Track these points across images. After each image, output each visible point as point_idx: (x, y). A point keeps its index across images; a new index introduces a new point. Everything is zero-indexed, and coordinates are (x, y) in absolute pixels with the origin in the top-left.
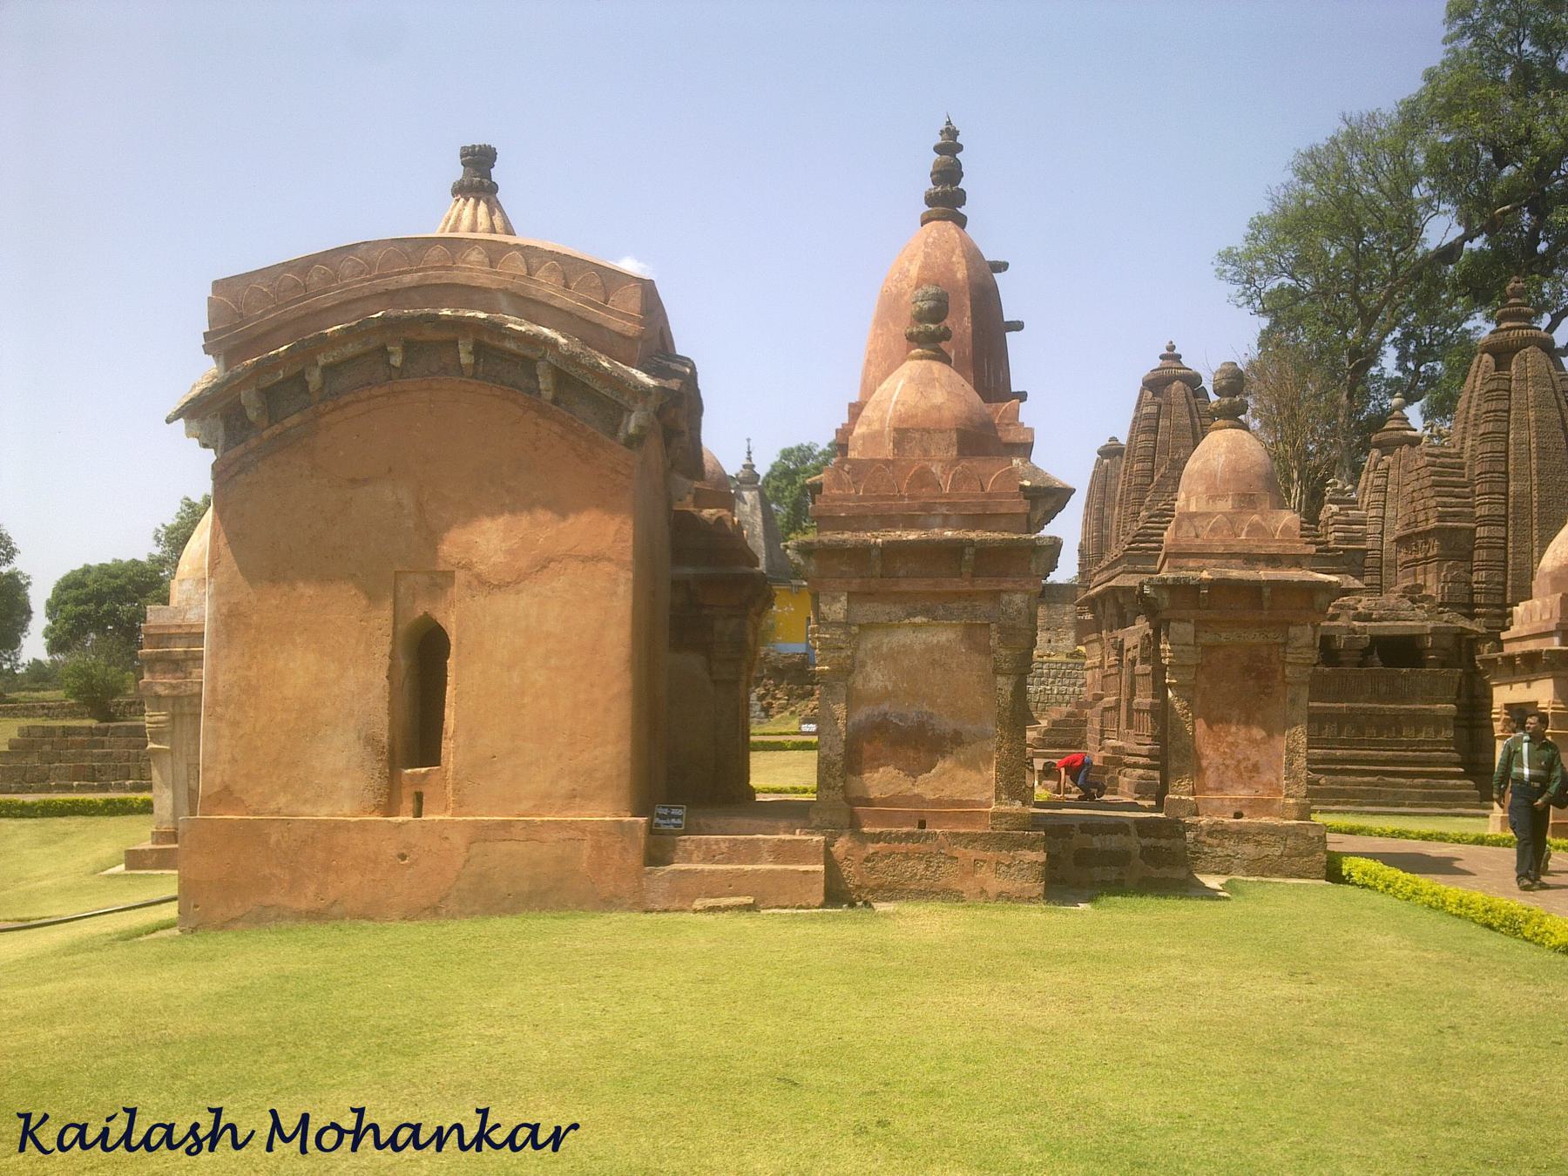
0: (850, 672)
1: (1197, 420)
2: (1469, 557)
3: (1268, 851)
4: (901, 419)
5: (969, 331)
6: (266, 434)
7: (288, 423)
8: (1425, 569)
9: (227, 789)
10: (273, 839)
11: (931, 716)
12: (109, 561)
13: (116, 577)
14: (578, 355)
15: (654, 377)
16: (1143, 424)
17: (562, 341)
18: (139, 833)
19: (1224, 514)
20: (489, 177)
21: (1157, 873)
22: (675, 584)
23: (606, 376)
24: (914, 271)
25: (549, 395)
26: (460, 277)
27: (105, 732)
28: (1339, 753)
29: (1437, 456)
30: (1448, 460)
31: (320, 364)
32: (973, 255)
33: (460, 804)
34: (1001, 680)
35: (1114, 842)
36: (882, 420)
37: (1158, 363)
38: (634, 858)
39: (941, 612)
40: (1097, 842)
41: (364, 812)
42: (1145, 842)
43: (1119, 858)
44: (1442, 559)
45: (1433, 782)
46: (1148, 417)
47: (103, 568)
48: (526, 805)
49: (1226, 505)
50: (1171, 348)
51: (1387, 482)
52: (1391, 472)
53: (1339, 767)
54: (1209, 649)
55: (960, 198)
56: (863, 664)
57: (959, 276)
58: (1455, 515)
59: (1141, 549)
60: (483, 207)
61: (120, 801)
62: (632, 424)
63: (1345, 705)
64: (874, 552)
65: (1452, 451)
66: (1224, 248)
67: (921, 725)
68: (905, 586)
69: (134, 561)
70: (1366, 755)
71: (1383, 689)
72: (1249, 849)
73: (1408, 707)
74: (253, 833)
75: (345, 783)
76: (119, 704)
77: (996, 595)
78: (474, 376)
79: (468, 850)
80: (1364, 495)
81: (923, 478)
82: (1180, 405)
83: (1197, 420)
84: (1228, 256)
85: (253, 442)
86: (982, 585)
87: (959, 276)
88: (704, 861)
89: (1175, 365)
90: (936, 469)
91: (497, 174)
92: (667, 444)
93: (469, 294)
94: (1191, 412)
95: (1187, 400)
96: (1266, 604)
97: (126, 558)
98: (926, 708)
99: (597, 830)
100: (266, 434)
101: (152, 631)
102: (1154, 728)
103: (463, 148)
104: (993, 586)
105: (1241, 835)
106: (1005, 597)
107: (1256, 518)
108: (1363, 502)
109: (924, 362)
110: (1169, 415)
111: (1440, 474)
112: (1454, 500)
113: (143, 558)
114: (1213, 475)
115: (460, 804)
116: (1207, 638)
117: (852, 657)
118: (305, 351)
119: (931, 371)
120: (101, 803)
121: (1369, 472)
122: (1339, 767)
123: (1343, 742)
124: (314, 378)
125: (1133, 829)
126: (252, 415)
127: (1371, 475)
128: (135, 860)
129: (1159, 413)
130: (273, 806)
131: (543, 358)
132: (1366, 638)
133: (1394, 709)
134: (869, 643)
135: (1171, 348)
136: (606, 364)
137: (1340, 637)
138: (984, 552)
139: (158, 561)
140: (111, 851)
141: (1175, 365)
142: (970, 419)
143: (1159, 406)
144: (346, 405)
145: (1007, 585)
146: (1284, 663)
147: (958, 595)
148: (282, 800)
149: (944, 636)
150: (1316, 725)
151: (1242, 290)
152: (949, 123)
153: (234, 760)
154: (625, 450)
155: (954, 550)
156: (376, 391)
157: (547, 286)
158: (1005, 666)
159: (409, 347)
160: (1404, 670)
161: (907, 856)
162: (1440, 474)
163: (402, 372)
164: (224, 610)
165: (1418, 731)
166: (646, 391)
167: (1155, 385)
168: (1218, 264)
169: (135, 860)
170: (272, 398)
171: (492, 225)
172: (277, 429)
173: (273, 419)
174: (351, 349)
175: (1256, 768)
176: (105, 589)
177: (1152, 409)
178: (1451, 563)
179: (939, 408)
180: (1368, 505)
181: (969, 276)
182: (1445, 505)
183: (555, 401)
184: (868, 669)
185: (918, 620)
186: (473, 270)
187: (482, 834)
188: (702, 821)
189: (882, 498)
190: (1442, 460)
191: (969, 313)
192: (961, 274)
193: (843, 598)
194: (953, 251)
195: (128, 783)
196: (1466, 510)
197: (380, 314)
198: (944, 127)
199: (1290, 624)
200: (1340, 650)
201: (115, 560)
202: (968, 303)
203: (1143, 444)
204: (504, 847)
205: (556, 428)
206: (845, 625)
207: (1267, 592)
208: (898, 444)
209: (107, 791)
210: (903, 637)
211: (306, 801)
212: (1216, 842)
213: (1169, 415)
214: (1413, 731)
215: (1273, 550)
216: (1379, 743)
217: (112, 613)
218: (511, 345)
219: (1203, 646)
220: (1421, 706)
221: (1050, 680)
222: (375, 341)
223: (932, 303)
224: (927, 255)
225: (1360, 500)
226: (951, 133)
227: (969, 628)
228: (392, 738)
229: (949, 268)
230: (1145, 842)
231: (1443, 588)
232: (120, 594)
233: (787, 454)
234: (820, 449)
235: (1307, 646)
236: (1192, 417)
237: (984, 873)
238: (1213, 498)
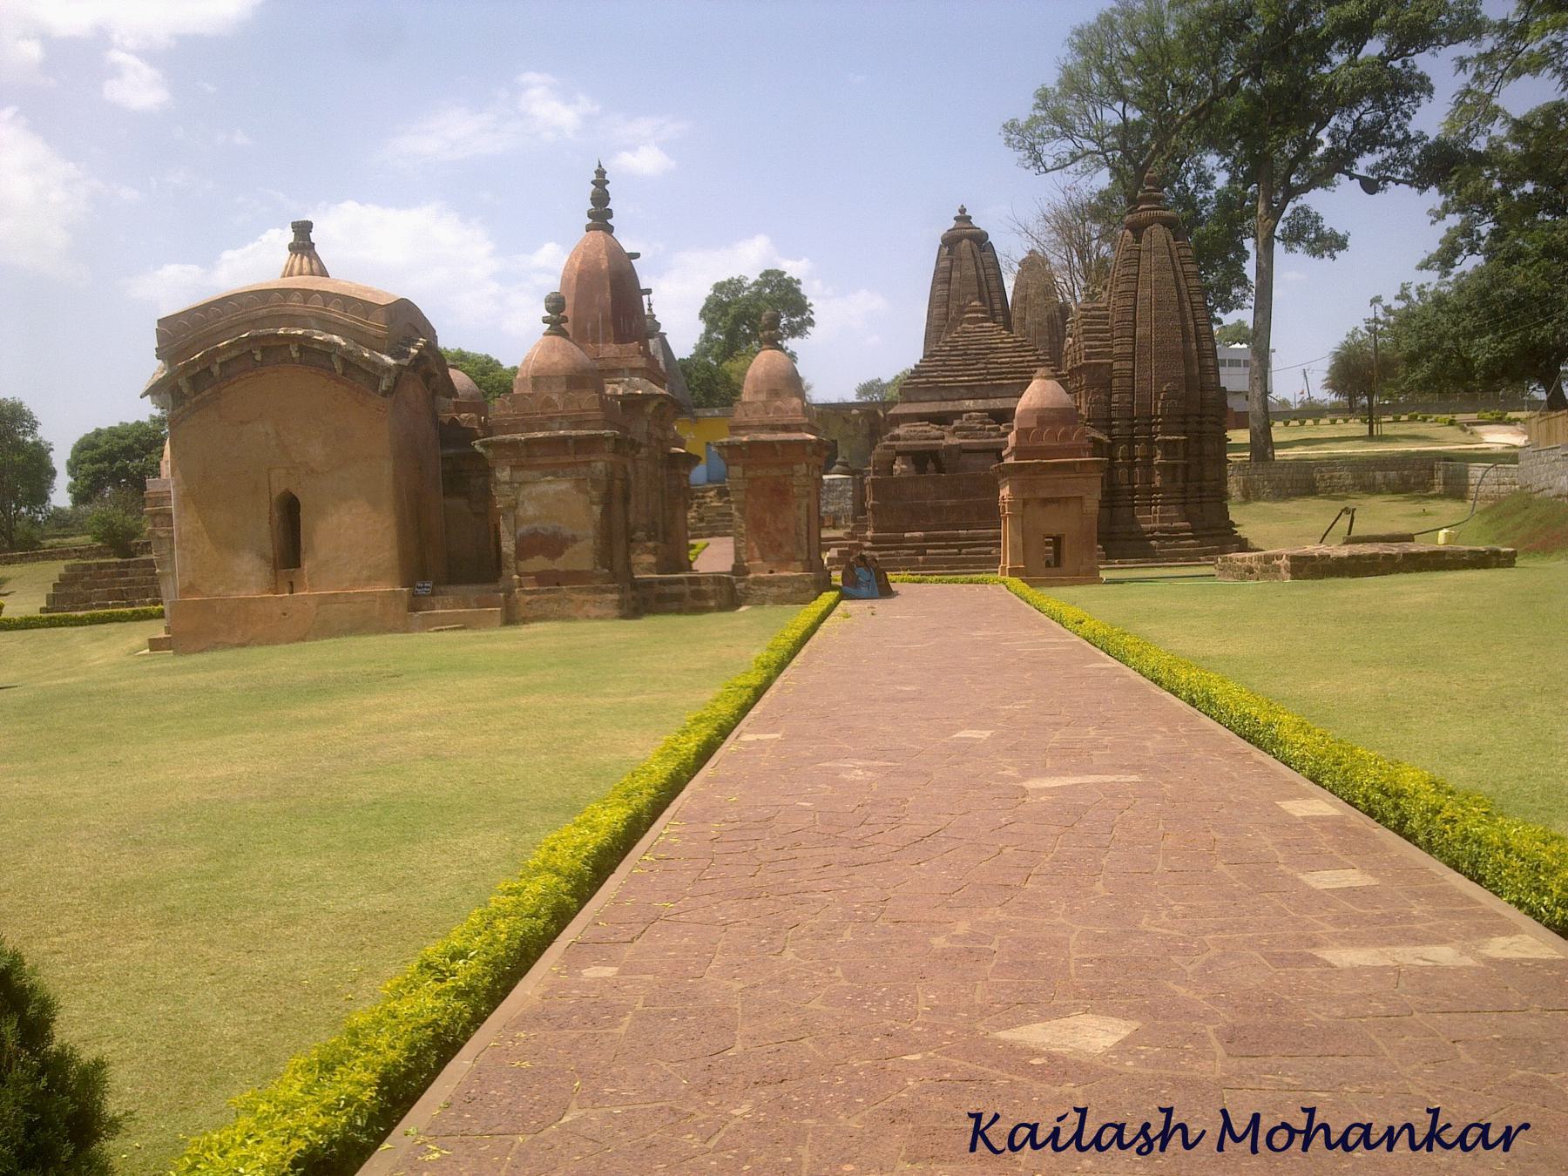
0: (515, 508)
3: (784, 590)
4: (536, 371)
6: (194, 400)
10: (218, 608)
11: (560, 528)
12: (117, 425)
15: (394, 358)
17: (343, 343)
20: (310, 240)
21: (699, 604)
22: (445, 459)
24: (577, 265)
26: (288, 310)
27: (127, 565)
29: (1089, 310)
30: (1097, 313)
32: (617, 253)
34: (595, 507)
35: (676, 589)
37: (952, 224)
39: (561, 473)
40: (667, 589)
41: (264, 593)
42: (693, 588)
43: (679, 597)
44: (1090, 386)
47: (112, 431)
48: (347, 584)
49: (762, 397)
50: (963, 210)
54: (752, 480)
55: (610, 214)
56: (523, 502)
57: (603, 267)
58: (1098, 354)
60: (306, 259)
61: (143, 611)
65: (1102, 305)
68: (539, 461)
69: (138, 422)
72: (775, 590)
75: (252, 579)
76: (138, 544)
77: (588, 463)
81: (548, 402)
84: (1011, 127)
86: (580, 458)
87: (603, 267)
88: (441, 608)
90: (555, 397)
92: (427, 383)
93: (293, 320)
97: (131, 421)
100: (194, 400)
101: (151, 496)
103: (293, 223)
104: (585, 458)
106: (593, 464)
107: (778, 403)
111: (1090, 324)
112: (1097, 343)
113: (145, 419)
115: (312, 586)
116: (750, 474)
117: (516, 500)
118: (209, 357)
119: (554, 341)
120: (130, 613)
124: (216, 370)
125: (686, 581)
126: (185, 391)
128: (155, 645)
130: (216, 592)
131: (334, 353)
134: (525, 491)
135: (963, 210)
136: (367, 355)
140: (139, 642)
141: (966, 226)
142: (575, 368)
143: (952, 261)
144: (234, 383)
145: (592, 458)
148: (221, 589)
149: (564, 485)
151: (1028, 155)
152: (600, 166)
153: (194, 570)
156: (250, 374)
157: (335, 313)
158: (596, 500)
159: (264, 350)
161: (548, 601)
162: (1090, 324)
163: (262, 363)
164: (181, 493)
166: (388, 369)
167: (950, 242)
169: (155, 645)
170: (194, 381)
171: (312, 269)
172: (199, 397)
173: (197, 392)
174: (234, 353)
175: (780, 545)
179: (556, 364)
181: (609, 267)
182: (1091, 347)
183: (344, 374)
184: (526, 505)
185: (549, 478)
187: (324, 600)
188: (442, 589)
189: (527, 414)
190: (1093, 313)
191: (609, 290)
192: (604, 266)
193: (508, 469)
194: (600, 251)
196: (1106, 350)
198: (597, 168)
199: (793, 463)
201: (121, 423)
202: (608, 283)
205: (345, 387)
206: (511, 483)
207: (778, 447)
209: (133, 606)
211: (233, 589)
217: (124, 469)
222: (246, 349)
223: (554, 304)
224: (585, 255)
226: (601, 173)
228: (274, 554)
229: (597, 263)
230: (693, 588)
232: (128, 452)
233: (719, 287)
234: (750, 282)
235: (804, 476)
236: (977, 269)
238: (756, 392)
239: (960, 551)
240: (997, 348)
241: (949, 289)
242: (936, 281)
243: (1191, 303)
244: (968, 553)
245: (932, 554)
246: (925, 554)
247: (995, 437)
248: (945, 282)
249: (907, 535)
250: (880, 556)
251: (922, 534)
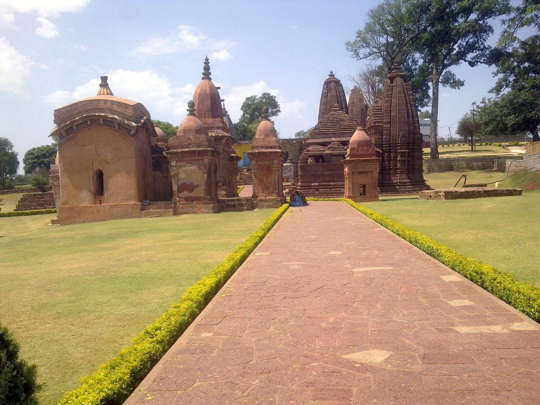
0: (177, 175)
3: (270, 203)
4: (185, 128)
5: (210, 104)
6: (67, 138)
7: (70, 136)
9: (66, 201)
10: (75, 209)
11: (193, 182)
12: (40, 146)
13: (42, 151)
14: (121, 121)
15: (136, 123)
17: (118, 118)
18: (54, 217)
19: (262, 138)
21: (241, 208)
22: (153, 158)
23: (126, 124)
25: (117, 128)
26: (99, 107)
27: (44, 195)
29: (375, 107)
30: (378, 108)
31: (75, 124)
33: (107, 202)
34: (205, 175)
35: (233, 203)
36: (181, 128)
37: (328, 77)
38: (138, 210)
40: (230, 203)
41: (91, 204)
43: (234, 206)
44: (375, 133)
47: (39, 149)
49: (263, 137)
50: (332, 72)
54: (259, 165)
55: (210, 74)
56: (180, 173)
57: (208, 92)
58: (378, 122)
59: (321, 132)
60: (105, 89)
62: (132, 133)
64: (179, 153)
66: (347, 41)
67: (191, 184)
68: (186, 159)
69: (47, 145)
72: (267, 203)
74: (71, 209)
75: (87, 199)
76: (47, 187)
77: (202, 160)
78: (104, 125)
79: (109, 210)
81: (189, 139)
85: (65, 139)
86: (200, 158)
87: (208, 92)
88: (152, 210)
89: (333, 78)
90: (191, 137)
91: (108, 81)
92: (147, 132)
93: (101, 110)
96: (268, 156)
97: (45, 145)
98: (192, 180)
99: (132, 205)
100: (67, 138)
103: (101, 77)
105: (265, 201)
106: (204, 160)
107: (268, 139)
109: (189, 116)
111: (375, 111)
112: (378, 118)
113: (50, 144)
114: (261, 130)
115: (107, 202)
116: (258, 163)
117: (178, 172)
118: (72, 123)
119: (191, 118)
120: (45, 211)
124: (74, 127)
126: (64, 135)
128: (53, 222)
129: (328, 92)
130: (74, 204)
134: (181, 169)
135: (332, 72)
136: (126, 122)
138: (199, 152)
139: (55, 145)
140: (48, 221)
141: (333, 78)
143: (328, 90)
144: (81, 132)
145: (204, 158)
146: (273, 167)
147: (196, 160)
149: (194, 167)
152: (207, 57)
154: (132, 137)
155: (194, 151)
157: (115, 108)
158: (205, 172)
159: (91, 120)
161: (189, 207)
162: (375, 111)
163: (90, 125)
164: (62, 170)
166: (134, 127)
167: (327, 83)
168: (346, 46)
169: (53, 222)
171: (107, 93)
173: (68, 135)
174: (81, 122)
175: (269, 188)
176: (40, 155)
179: (191, 125)
181: (210, 92)
183: (119, 129)
185: (189, 165)
186: (102, 105)
187: (112, 207)
189: (181, 143)
190: (376, 108)
191: (210, 100)
192: (208, 92)
195: (51, 207)
196: (381, 120)
197: (85, 115)
198: (205, 58)
199: (273, 160)
201: (42, 146)
204: (116, 209)
205: (119, 134)
207: (268, 154)
208: (184, 132)
209: (46, 209)
210: (187, 168)
211: (80, 203)
212: (260, 202)
215: (271, 145)
217: (43, 162)
218: (109, 119)
219: (258, 165)
222: (85, 120)
223: (191, 105)
224: (201, 88)
226: (207, 59)
227: (199, 166)
228: (95, 191)
229: (206, 90)
232: (44, 156)
233: (248, 99)
234: (258, 97)
235: (277, 164)
236: (337, 93)
237: (202, 209)
239: (331, 190)
241: (327, 100)
242: (322, 97)
244: (333, 191)
245: (321, 191)
246: (318, 191)
248: (325, 97)
249: (312, 184)
250: (303, 191)
251: (317, 184)
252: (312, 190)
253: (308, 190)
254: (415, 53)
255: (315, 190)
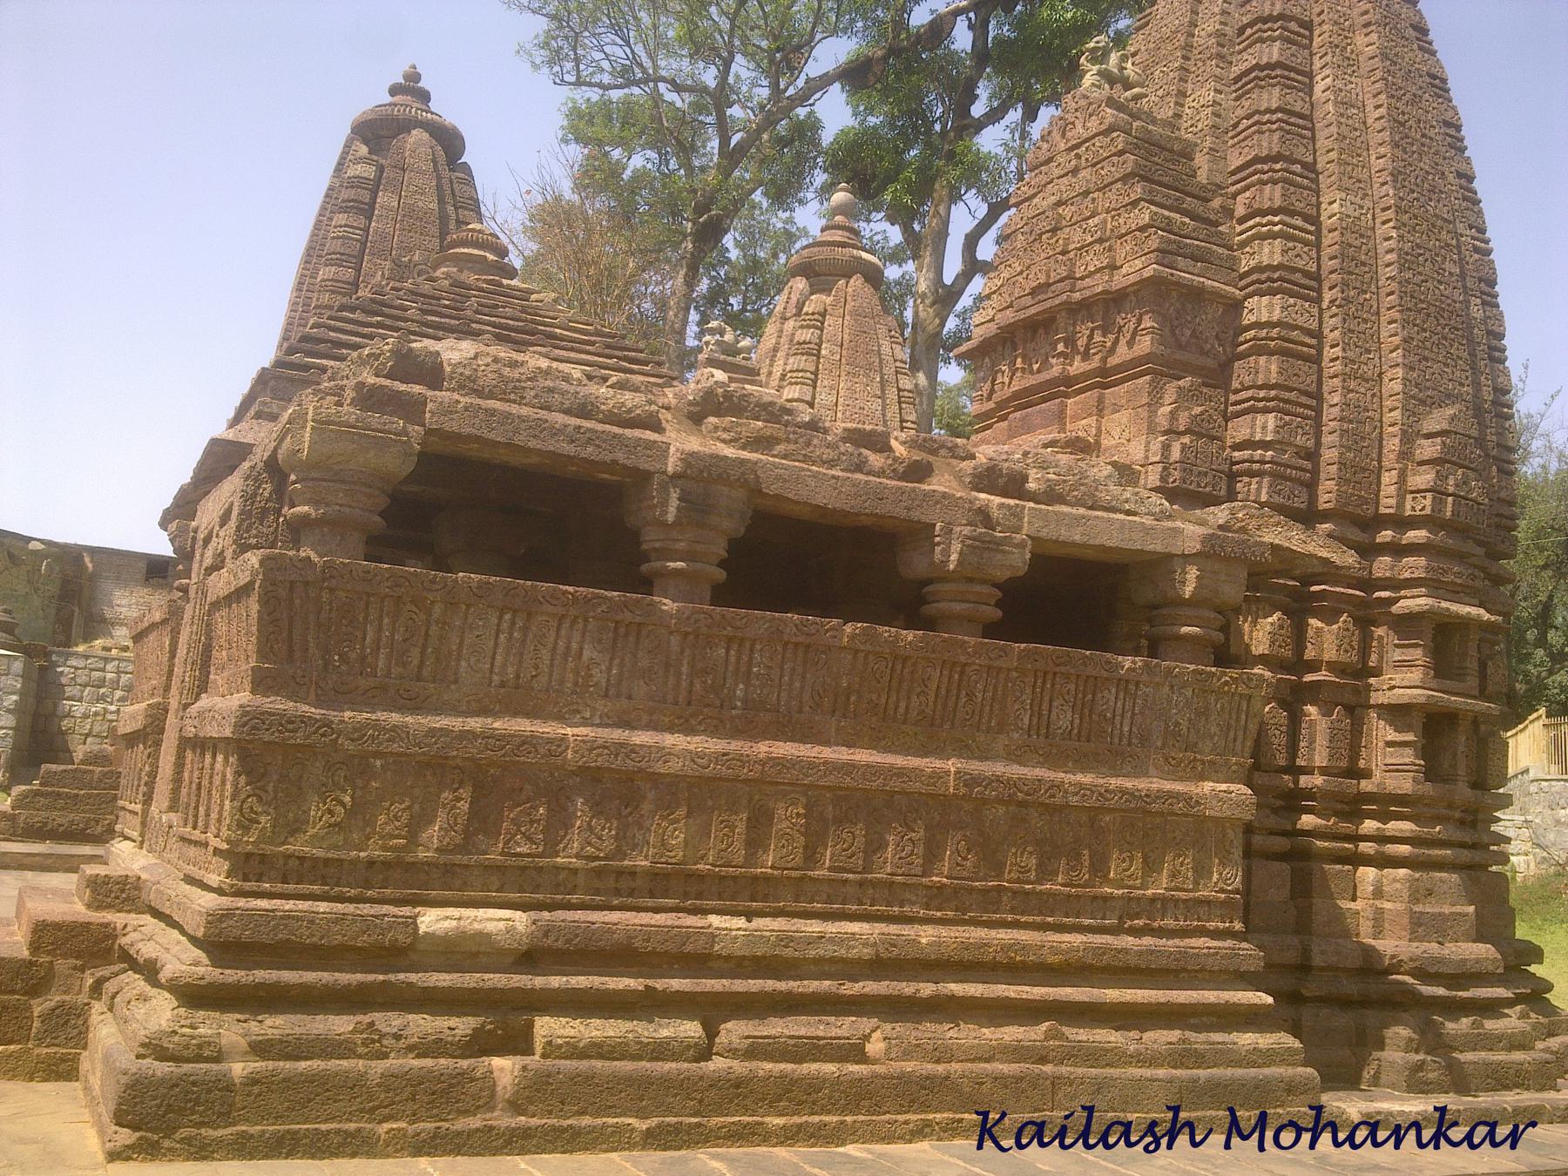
1: (450, 209)
2: (1218, 376)
8: (1101, 400)
16: (345, 194)
28: (926, 935)
44: (1161, 368)
45: (1199, 1039)
46: (356, 183)
51: (820, 337)
52: (829, 320)
53: (927, 989)
63: (952, 765)
70: (1006, 948)
71: (1064, 719)
73: (1128, 784)
80: (772, 361)
82: (424, 173)
83: (450, 209)
94: (439, 187)
95: (436, 169)
102: (245, 822)
108: (770, 373)
110: (398, 188)
121: (784, 319)
122: (927, 989)
123: (937, 897)
127: (790, 324)
132: (1022, 545)
133: (1091, 788)
137: (948, 531)
150: (859, 830)
160: (1127, 662)
165: (1151, 867)
177: (369, 171)
178: (1185, 382)
180: (783, 376)
200: (947, 578)
203: (339, 232)
213: (398, 188)
214: (1136, 866)
216: (1047, 903)
220: (1168, 786)
221: (119, 693)
225: (764, 371)
231: (1166, 447)
236: (441, 201)
239: (711, 1033)
240: (555, 337)
241: (367, 230)
242: (332, 203)
243: (899, 390)
244: (754, 1051)
245: (576, 1051)
246: (518, 1043)
247: (880, 473)
248: (360, 211)
249: (432, 921)
250: (260, 1049)
251: (520, 920)
252: (422, 1024)
253: (341, 1025)
254: (419, 356)
255: (463, 1025)
